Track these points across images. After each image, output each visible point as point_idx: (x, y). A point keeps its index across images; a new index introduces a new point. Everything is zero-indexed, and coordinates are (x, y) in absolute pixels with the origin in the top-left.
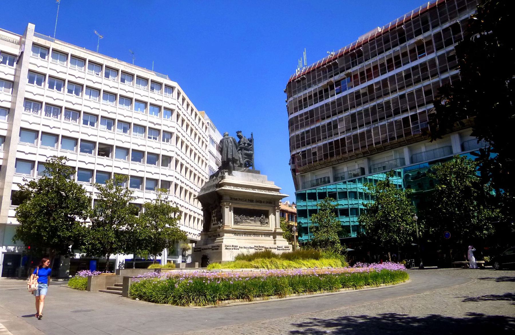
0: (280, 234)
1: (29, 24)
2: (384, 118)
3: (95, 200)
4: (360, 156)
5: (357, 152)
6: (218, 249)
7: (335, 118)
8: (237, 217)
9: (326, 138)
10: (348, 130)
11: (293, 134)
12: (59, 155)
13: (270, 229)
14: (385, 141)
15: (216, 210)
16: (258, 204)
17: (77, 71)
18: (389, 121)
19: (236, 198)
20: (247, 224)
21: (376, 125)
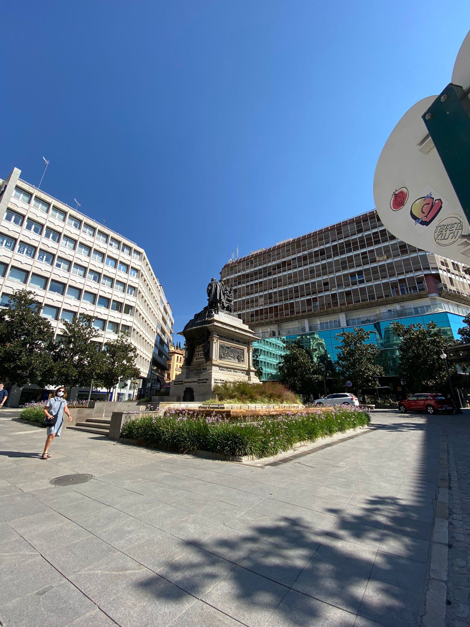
1: (16, 168)
3: (58, 335)
6: (206, 382)
7: (257, 295)
10: (266, 304)
12: (28, 289)
13: (244, 366)
15: (203, 345)
19: (222, 335)
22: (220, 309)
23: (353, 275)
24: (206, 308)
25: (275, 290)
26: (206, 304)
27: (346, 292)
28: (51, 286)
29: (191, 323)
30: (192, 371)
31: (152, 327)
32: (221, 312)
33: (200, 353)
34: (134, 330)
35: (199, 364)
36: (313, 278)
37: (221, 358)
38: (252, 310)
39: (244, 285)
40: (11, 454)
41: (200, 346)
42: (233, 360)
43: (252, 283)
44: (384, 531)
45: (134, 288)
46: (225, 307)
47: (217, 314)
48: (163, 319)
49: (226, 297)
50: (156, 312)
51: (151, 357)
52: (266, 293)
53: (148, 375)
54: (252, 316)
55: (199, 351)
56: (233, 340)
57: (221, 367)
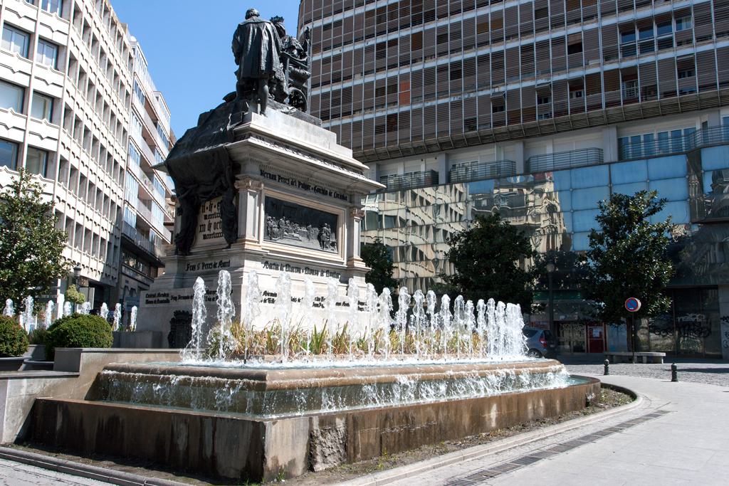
0: (359, 272)
4: (435, 148)
8: (272, 223)
9: (383, 105)
15: (220, 199)
16: (319, 195)
19: (272, 172)
20: (293, 242)
22: (270, 99)
23: (627, 29)
24: (229, 98)
25: (444, 61)
26: (231, 85)
27: (624, 70)
29: (192, 139)
30: (193, 268)
31: (116, 157)
32: (275, 107)
33: (213, 221)
34: (63, 161)
35: (210, 253)
37: (270, 235)
38: (379, 114)
39: (359, 46)
40: (381, 443)
41: (215, 202)
42: (305, 242)
43: (380, 39)
45: (58, 47)
46: (285, 95)
47: (262, 112)
48: (146, 136)
49: (289, 66)
50: (124, 115)
51: (110, 228)
53: (105, 275)
55: (211, 216)
56: (306, 187)
57: (271, 262)
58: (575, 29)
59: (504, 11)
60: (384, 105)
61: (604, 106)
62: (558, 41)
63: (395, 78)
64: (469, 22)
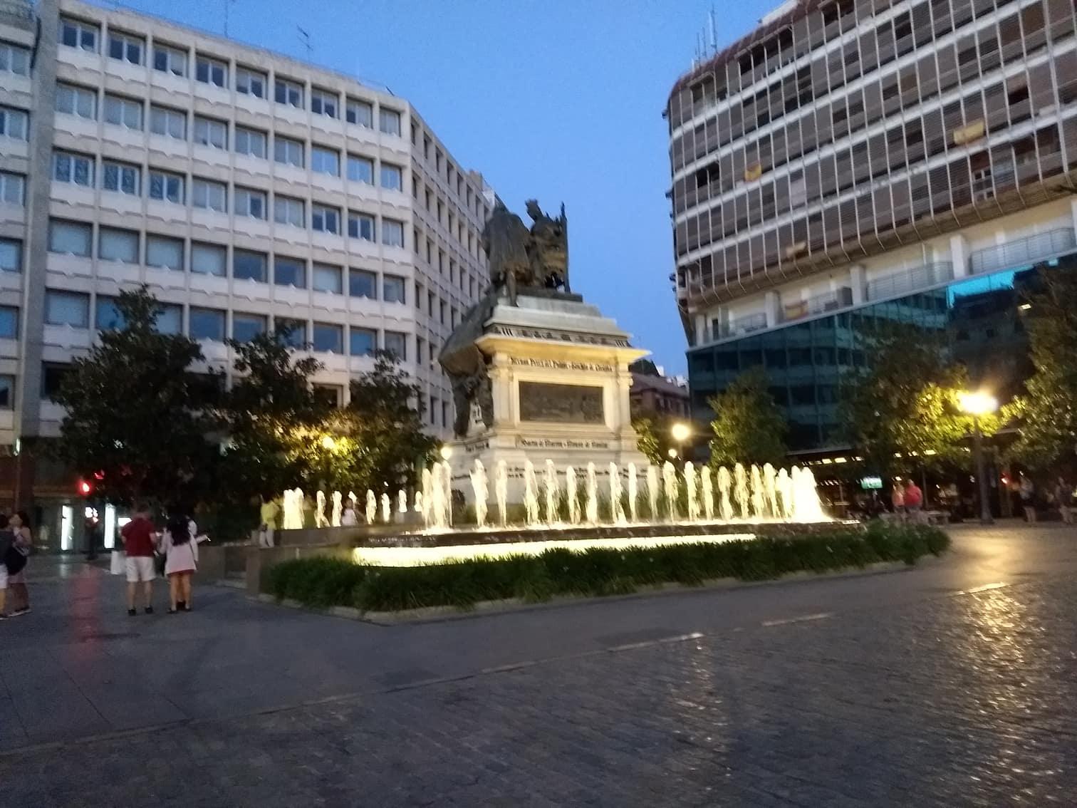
2: (902, 165)
5: (835, 250)
7: (783, 172)
10: (813, 199)
11: (682, 218)
14: (885, 227)
17: (121, 211)
18: (916, 171)
21: (884, 184)
28: (235, 261)
36: (970, 78)
39: (740, 144)
44: (315, 498)
52: (811, 159)
54: (920, 193)
58: (1016, 69)
59: (936, 55)
60: (760, 221)
61: (1066, 169)
62: (995, 90)
63: (917, 121)
64: (872, 88)
